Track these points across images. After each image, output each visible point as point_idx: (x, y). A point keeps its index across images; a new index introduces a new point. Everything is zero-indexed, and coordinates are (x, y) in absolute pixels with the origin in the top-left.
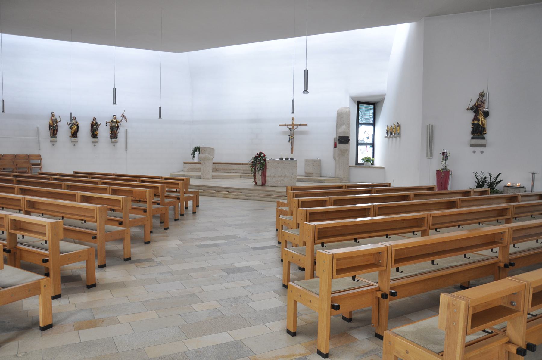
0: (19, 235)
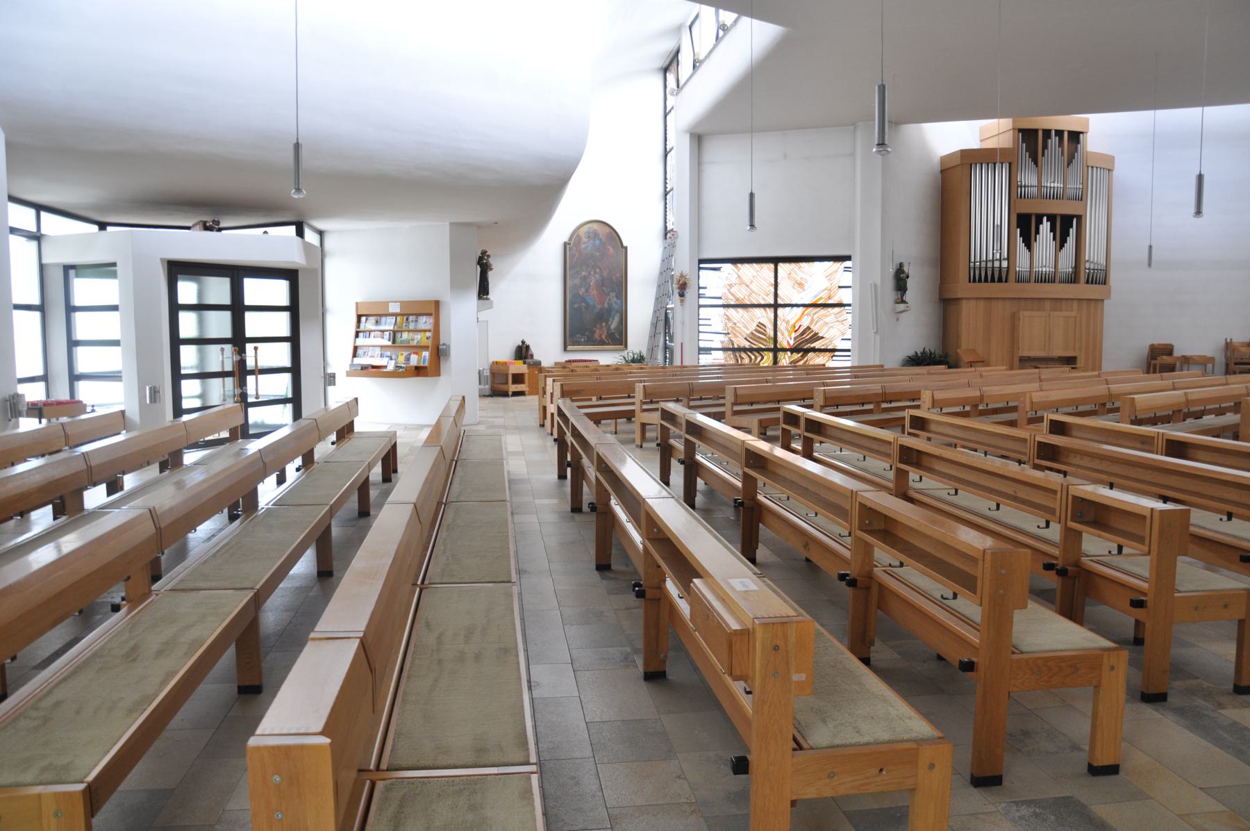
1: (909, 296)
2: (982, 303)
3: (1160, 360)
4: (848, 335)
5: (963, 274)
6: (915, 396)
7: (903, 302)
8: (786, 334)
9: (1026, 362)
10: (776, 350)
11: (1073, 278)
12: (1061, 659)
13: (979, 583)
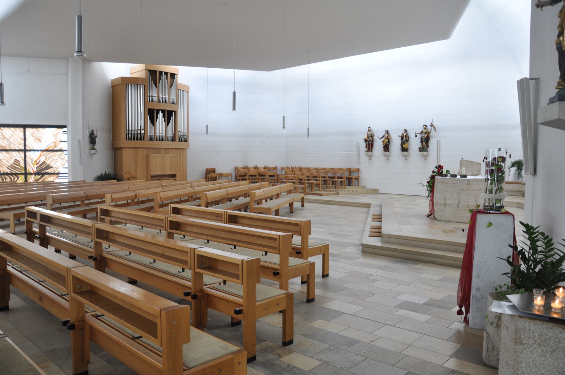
0: (105, 245)
1: (96, 146)
2: (132, 150)
3: (211, 175)
4: (66, 165)
5: (123, 136)
6: (102, 196)
7: (94, 149)
8: (32, 165)
9: (155, 177)
10: (26, 174)
11: (173, 139)
12: (212, 367)
13: (159, 327)
